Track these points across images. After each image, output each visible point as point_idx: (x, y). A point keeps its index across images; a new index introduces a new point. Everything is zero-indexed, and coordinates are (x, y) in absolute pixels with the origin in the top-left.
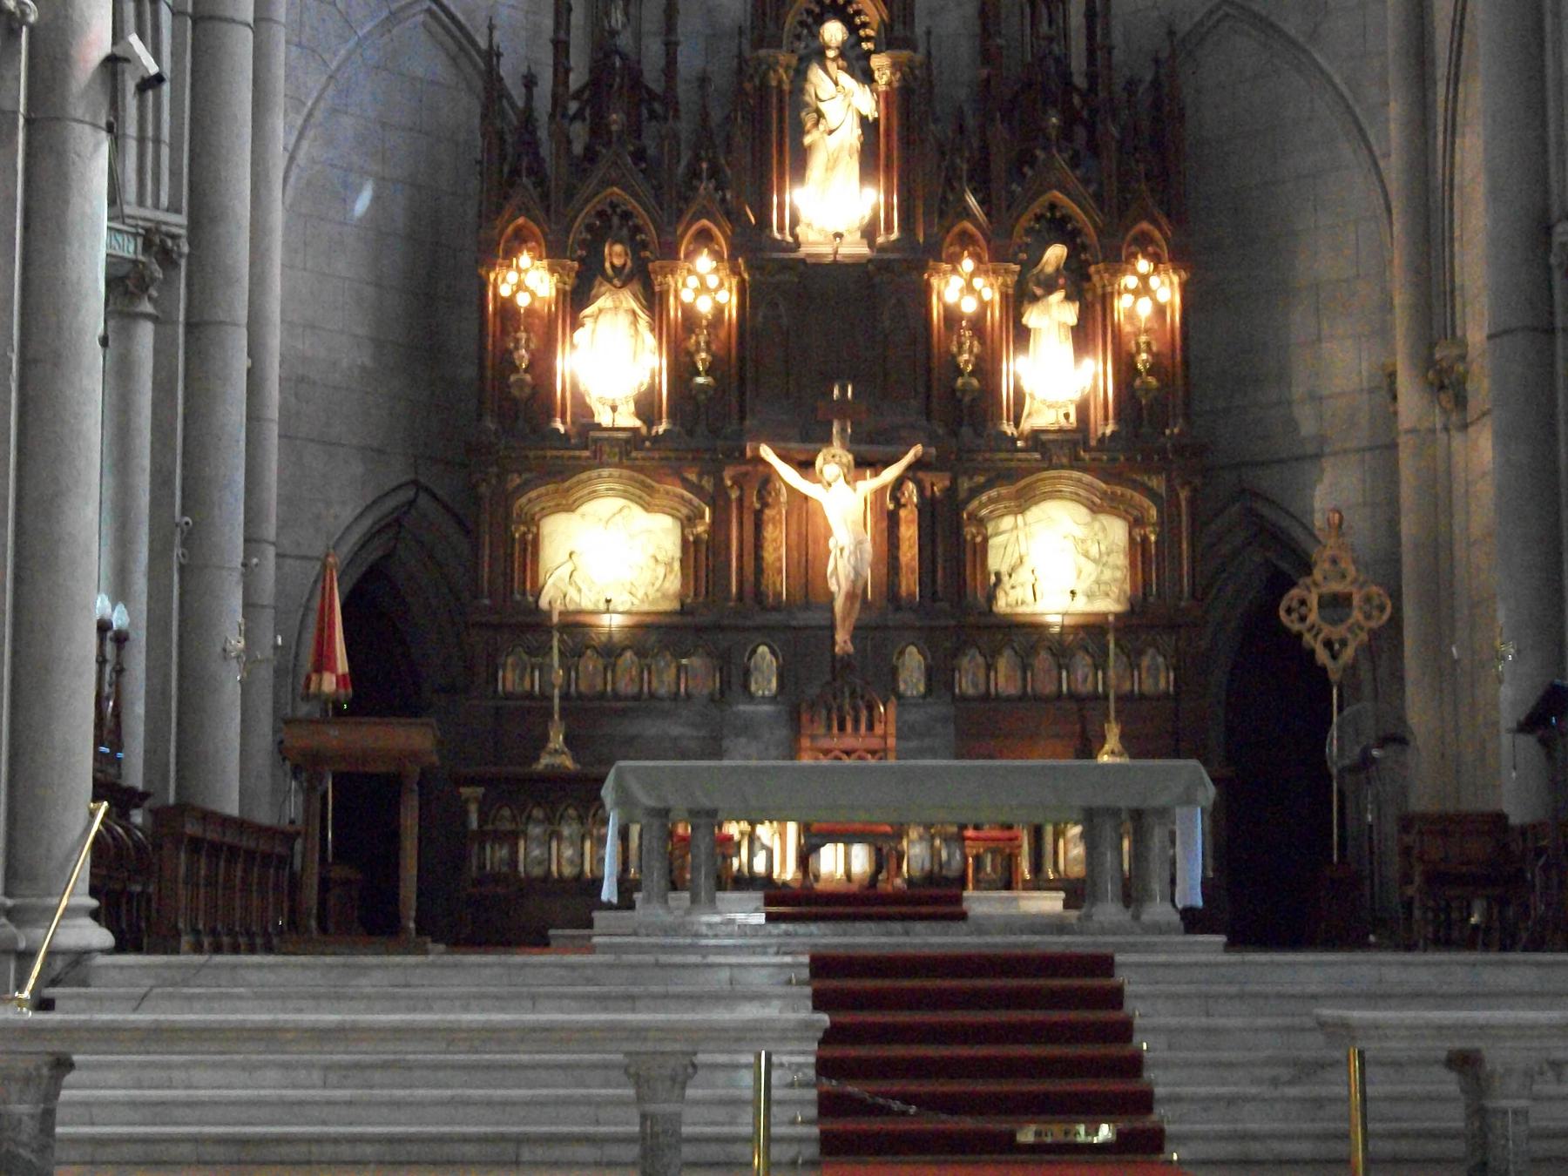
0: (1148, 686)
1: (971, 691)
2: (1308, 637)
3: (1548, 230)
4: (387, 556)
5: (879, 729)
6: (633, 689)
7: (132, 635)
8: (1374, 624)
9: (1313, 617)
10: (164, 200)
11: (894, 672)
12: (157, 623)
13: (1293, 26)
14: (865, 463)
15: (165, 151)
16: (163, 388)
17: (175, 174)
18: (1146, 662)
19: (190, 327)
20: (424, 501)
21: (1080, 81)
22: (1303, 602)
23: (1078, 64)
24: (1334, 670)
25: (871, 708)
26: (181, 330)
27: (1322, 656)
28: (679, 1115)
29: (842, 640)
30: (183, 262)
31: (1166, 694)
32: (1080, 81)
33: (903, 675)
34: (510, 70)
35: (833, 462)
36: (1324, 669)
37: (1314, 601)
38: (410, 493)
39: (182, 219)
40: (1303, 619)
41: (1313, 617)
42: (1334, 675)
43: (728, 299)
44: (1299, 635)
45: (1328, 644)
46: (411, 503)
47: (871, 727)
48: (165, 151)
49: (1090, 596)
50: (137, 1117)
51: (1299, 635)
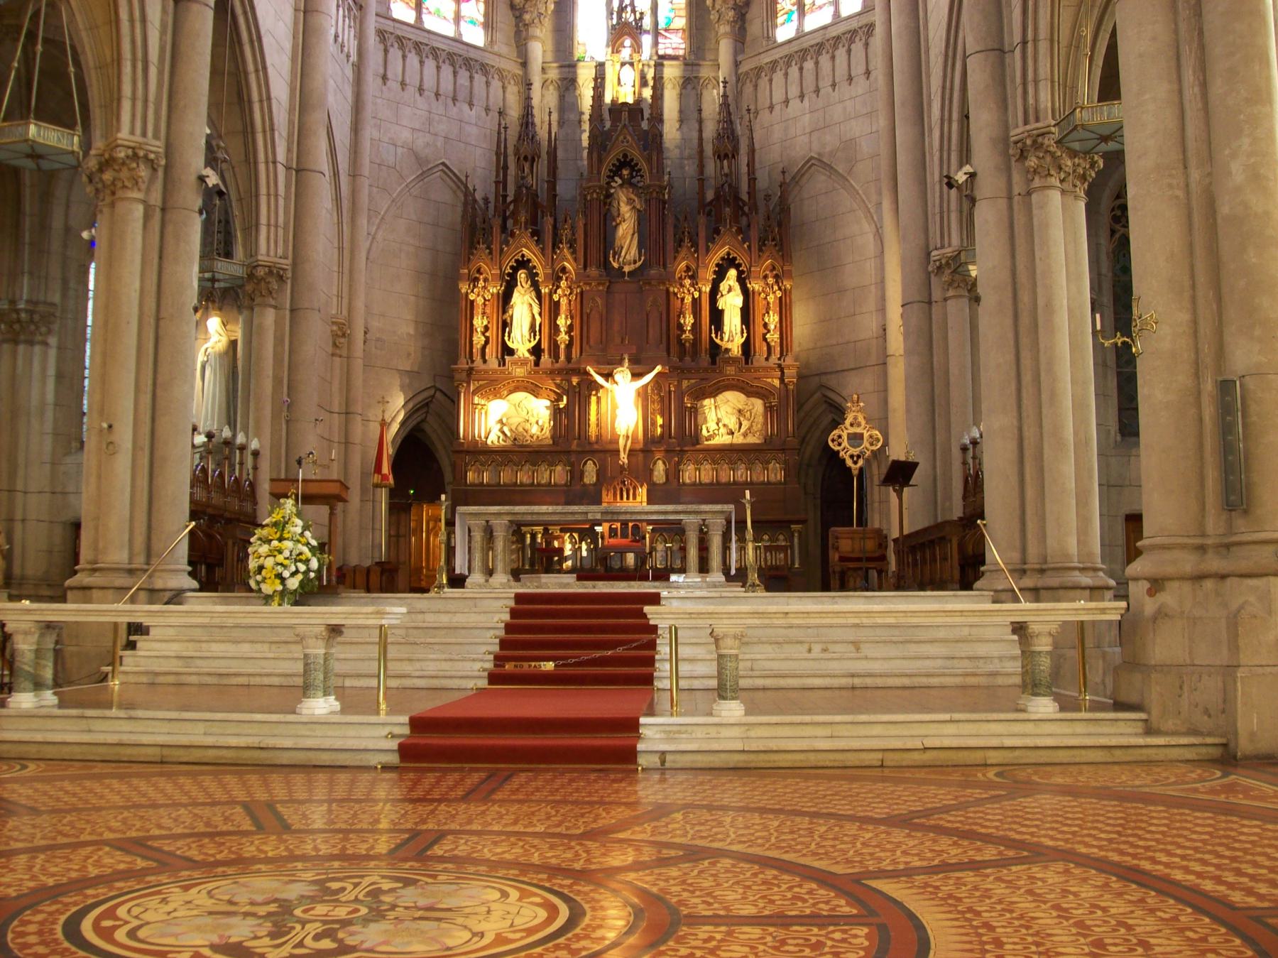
0: (772, 478)
1: (688, 481)
2: (842, 454)
3: (929, 254)
4: (423, 421)
5: (639, 499)
6: (529, 481)
7: (262, 452)
8: (875, 448)
9: (845, 443)
10: (280, 252)
11: (651, 471)
12: (275, 447)
13: (840, 168)
14: (636, 375)
15: (281, 232)
16: (279, 341)
17: (286, 241)
18: (771, 466)
19: (292, 311)
20: (438, 395)
21: (745, 197)
22: (840, 437)
23: (744, 187)
24: (855, 468)
25: (635, 489)
26: (288, 313)
27: (849, 463)
28: (490, 683)
29: (624, 458)
30: (289, 282)
31: (780, 483)
32: (745, 197)
33: (656, 473)
34: (478, 196)
35: (623, 375)
36: (850, 469)
37: (845, 437)
38: (432, 392)
39: (289, 261)
40: (840, 444)
41: (845, 443)
42: (855, 472)
43: (461, 285)
44: (838, 452)
45: (852, 457)
46: (433, 396)
47: (634, 498)
48: (281, 232)
49: (745, 435)
50: (1129, 730)
51: (838, 452)
